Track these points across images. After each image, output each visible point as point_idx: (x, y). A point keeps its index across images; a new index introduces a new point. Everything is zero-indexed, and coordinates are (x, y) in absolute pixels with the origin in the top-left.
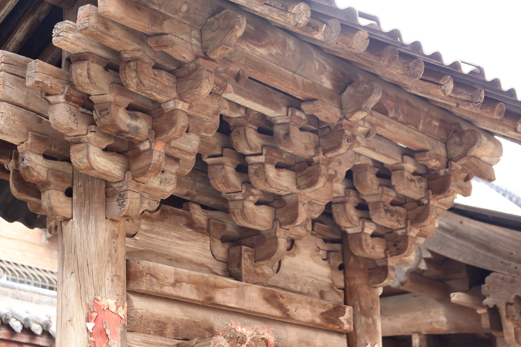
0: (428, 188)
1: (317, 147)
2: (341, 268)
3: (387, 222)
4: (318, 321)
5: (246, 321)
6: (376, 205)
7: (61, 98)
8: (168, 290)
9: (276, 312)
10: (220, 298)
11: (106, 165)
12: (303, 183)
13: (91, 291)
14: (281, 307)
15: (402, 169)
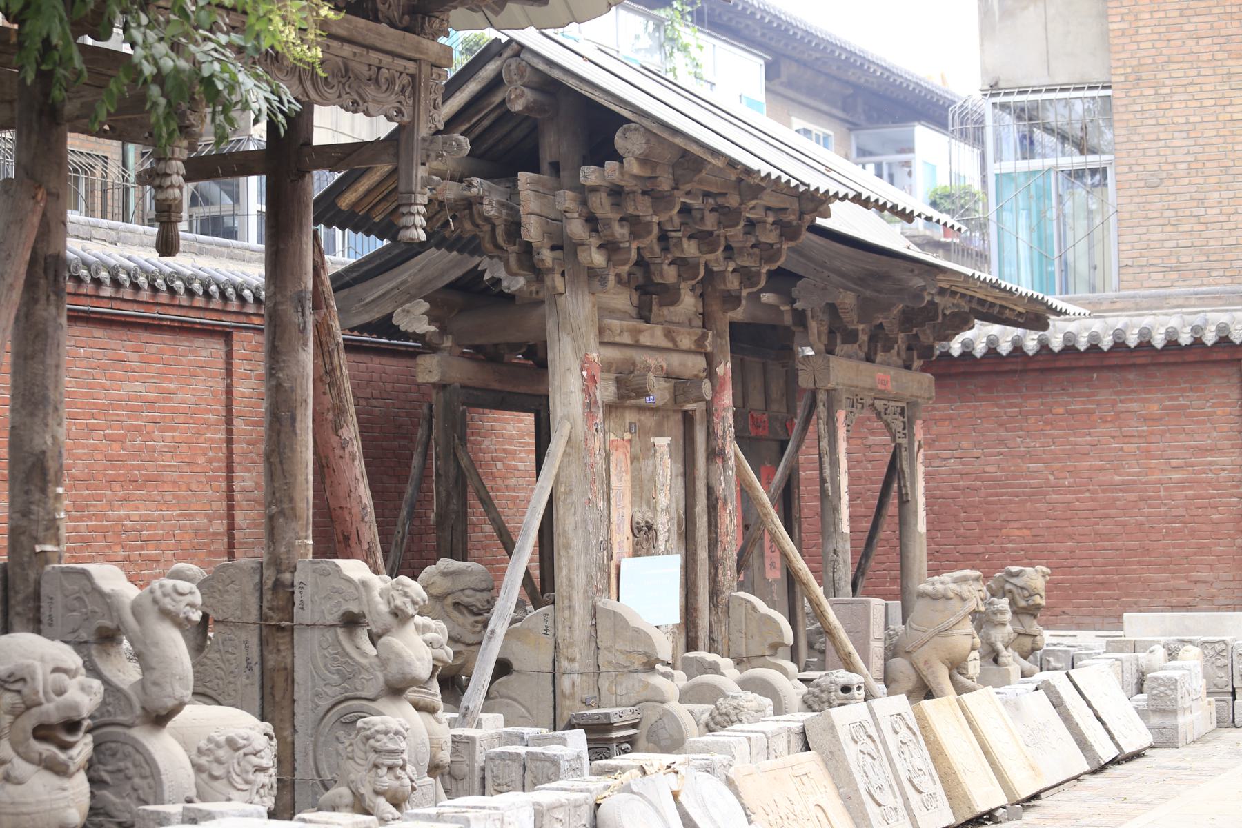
0: (781, 235)
1: (719, 223)
2: (702, 295)
3: (745, 261)
4: (693, 347)
5: (651, 353)
6: (741, 250)
7: (576, 215)
8: (617, 339)
9: (670, 345)
10: (645, 339)
11: (598, 259)
12: (705, 249)
13: (583, 347)
14: (673, 341)
15: (765, 222)
